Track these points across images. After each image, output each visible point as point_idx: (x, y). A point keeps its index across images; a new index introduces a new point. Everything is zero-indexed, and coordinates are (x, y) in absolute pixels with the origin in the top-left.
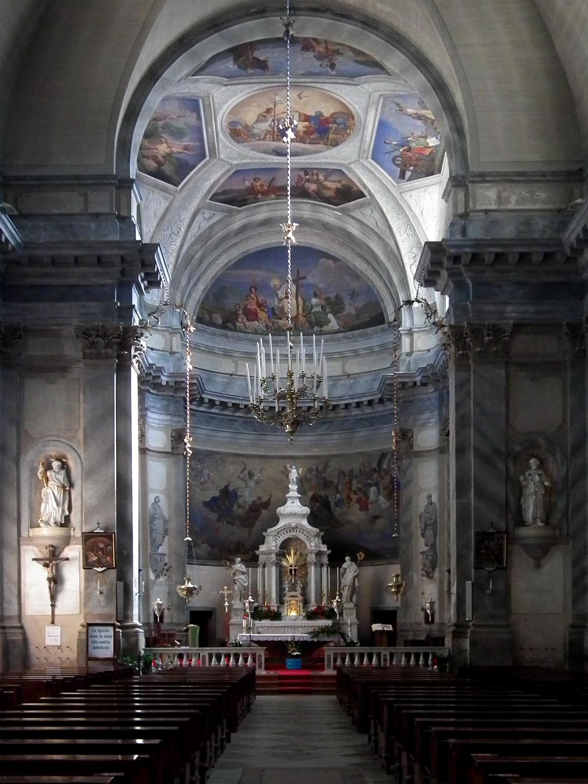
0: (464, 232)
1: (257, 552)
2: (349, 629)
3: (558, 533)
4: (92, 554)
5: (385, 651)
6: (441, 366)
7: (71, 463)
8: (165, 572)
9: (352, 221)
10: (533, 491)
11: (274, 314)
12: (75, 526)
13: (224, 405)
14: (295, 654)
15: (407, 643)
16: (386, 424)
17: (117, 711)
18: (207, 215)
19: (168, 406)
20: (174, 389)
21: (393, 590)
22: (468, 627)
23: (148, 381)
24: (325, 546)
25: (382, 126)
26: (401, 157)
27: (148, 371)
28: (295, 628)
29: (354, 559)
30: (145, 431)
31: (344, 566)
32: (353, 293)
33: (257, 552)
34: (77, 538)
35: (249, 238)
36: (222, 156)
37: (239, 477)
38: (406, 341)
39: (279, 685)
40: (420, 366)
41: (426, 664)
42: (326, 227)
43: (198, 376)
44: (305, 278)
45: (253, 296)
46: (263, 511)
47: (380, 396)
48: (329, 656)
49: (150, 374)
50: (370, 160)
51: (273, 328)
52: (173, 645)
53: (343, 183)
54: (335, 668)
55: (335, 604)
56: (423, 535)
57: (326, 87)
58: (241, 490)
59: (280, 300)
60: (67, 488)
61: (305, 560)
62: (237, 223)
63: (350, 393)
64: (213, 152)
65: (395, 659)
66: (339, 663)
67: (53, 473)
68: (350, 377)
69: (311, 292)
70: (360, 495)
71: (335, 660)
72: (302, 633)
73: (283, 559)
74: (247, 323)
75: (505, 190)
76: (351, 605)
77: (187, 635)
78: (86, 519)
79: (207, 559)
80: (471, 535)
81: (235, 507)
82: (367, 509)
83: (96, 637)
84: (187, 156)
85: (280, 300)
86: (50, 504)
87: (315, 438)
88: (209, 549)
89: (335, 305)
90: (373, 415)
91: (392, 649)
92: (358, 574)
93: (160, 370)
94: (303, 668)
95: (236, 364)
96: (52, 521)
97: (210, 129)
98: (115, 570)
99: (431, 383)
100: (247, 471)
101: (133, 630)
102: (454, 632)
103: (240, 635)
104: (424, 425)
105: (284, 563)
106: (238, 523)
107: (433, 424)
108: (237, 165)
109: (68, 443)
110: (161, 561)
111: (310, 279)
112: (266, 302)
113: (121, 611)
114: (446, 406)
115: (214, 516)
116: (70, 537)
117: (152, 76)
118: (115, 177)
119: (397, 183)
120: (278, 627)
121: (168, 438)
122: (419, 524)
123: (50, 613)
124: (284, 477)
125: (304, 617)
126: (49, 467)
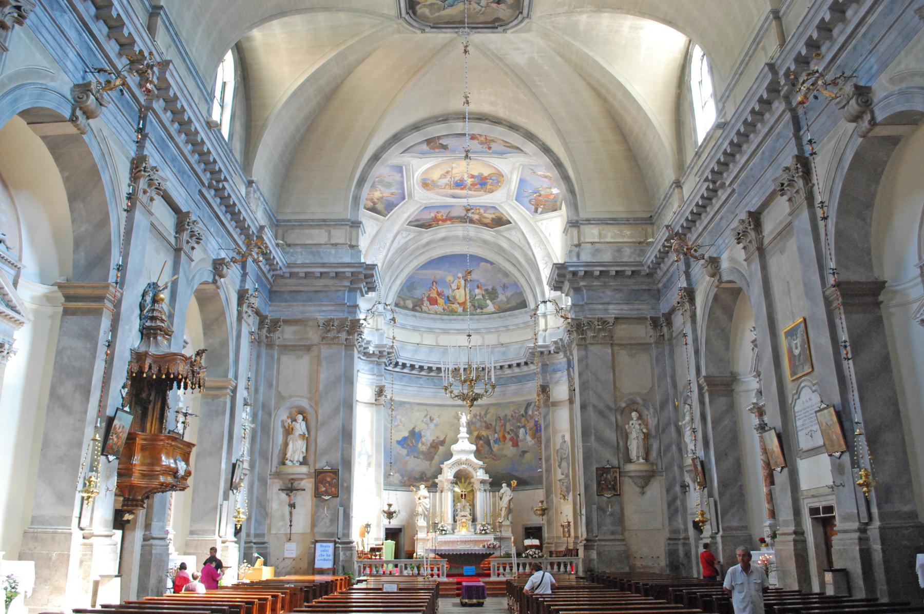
0: (578, 256)
1: (436, 480)
3: (655, 468)
9: (503, 239)
25: (522, 181)
29: (509, 485)
31: (502, 491)
36: (416, 198)
38: (542, 321)
42: (485, 242)
46: (440, 447)
47: (525, 360)
53: (497, 215)
57: (486, 159)
63: (504, 358)
64: (410, 196)
69: (475, 285)
70: (512, 435)
74: (431, 307)
75: (603, 230)
81: (420, 445)
84: (393, 199)
88: (401, 478)
89: (492, 294)
95: (422, 336)
100: (428, 417)
102: (585, 546)
104: (557, 382)
115: (404, 452)
117: (376, 158)
118: (349, 220)
124: (456, 421)
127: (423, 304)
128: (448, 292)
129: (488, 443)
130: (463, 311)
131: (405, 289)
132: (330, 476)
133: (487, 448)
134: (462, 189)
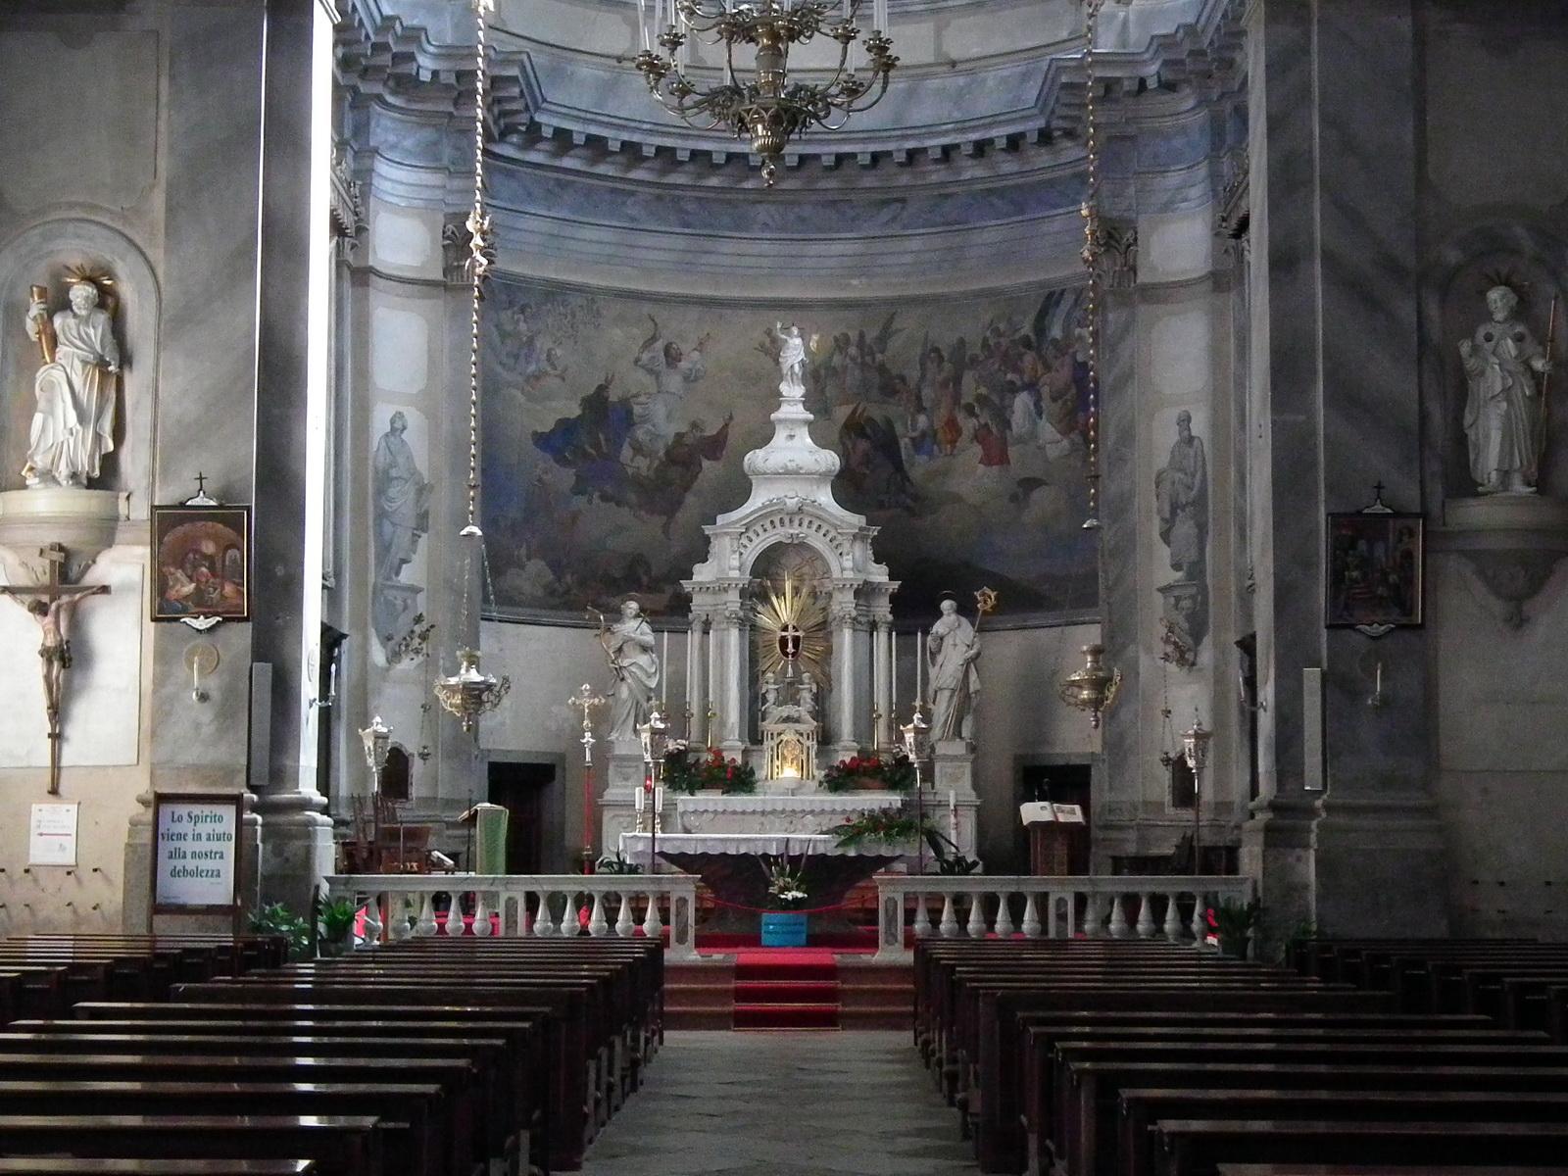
1: (687, 585)
2: (953, 820)
4: (179, 574)
5: (1062, 889)
6: (1218, 28)
7: (127, 291)
8: (417, 641)
10: (1498, 388)
12: (132, 485)
13: (596, 146)
14: (790, 896)
15: (1119, 865)
16: (1056, 206)
17: (236, 1087)
19: (435, 144)
20: (456, 93)
21: (1085, 694)
22: (1312, 813)
23: (380, 69)
24: (884, 568)
27: (380, 39)
28: (792, 816)
29: (966, 609)
30: (368, 216)
31: (939, 627)
33: (687, 585)
34: (136, 524)
37: (637, 361)
39: (742, 995)
40: (1156, 33)
41: (1186, 933)
43: (525, 57)
46: (706, 463)
47: (1041, 123)
48: (892, 901)
49: (385, 47)
52: (430, 865)
54: (910, 941)
55: (909, 737)
56: (1166, 536)
58: (642, 399)
60: (111, 368)
61: (824, 609)
63: (957, 115)
65: (1090, 915)
66: (920, 926)
67: (72, 321)
68: (959, 67)
70: (985, 417)
71: (910, 916)
72: (813, 833)
73: (760, 608)
76: (958, 748)
77: (470, 839)
78: (163, 466)
79: (542, 607)
80: (1318, 523)
81: (626, 452)
82: (1002, 459)
83: (182, 837)
86: (59, 412)
90: (1021, 181)
91: (1081, 883)
92: (978, 654)
93: (414, 35)
94: (814, 941)
96: (63, 471)
98: (249, 626)
99: (1188, 81)
100: (660, 345)
101: (298, 817)
102: (1269, 829)
103: (624, 839)
104: (1167, 207)
105: (765, 620)
106: (632, 497)
107: (1198, 202)
109: (120, 228)
110: (405, 608)
113: (262, 755)
114: (1231, 149)
115: (564, 478)
116: (116, 519)
120: (743, 813)
121: (433, 241)
122: (1155, 504)
123: (48, 762)
124: (769, 363)
125: (821, 783)
126: (59, 302)
132: (215, 537)
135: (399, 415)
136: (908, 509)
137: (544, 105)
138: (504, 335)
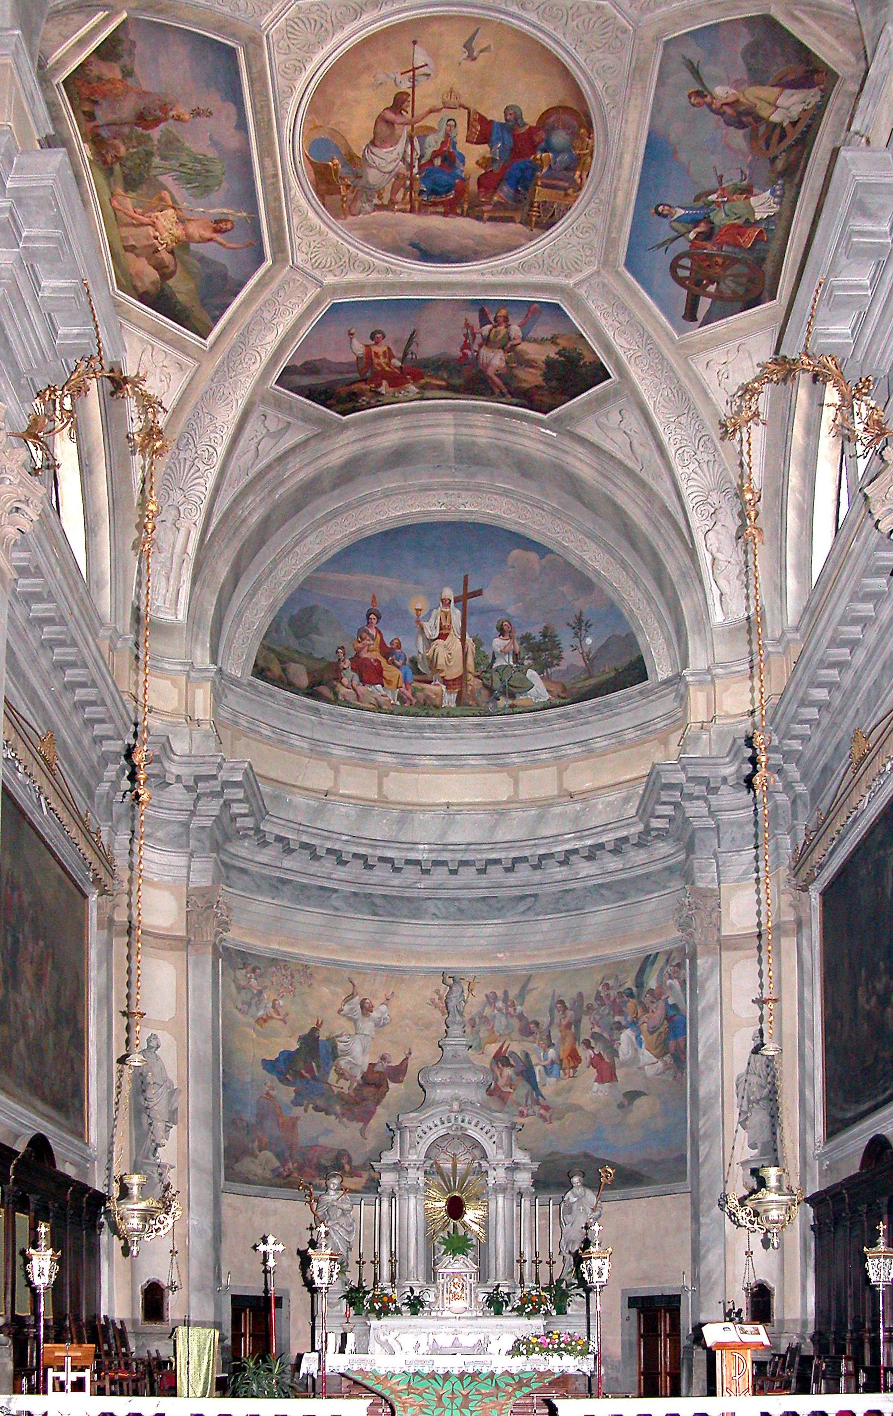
11: (417, 671)
16: (652, 892)
18: (273, 425)
26: (690, 257)
32: (579, 620)
35: (362, 502)
37: (340, 1011)
44: (479, 593)
45: (373, 632)
46: (391, 1085)
50: (622, 269)
51: (414, 701)
56: (743, 1123)
58: (344, 1038)
59: (430, 641)
62: (338, 454)
68: (576, 798)
69: (493, 626)
74: (361, 689)
81: (332, 1077)
82: (612, 1077)
85: (430, 641)
87: (501, 930)
88: (277, 1164)
95: (337, 771)
97: (268, 162)
100: (357, 1000)
106: (338, 1108)
108: (334, 290)
111: (489, 598)
112: (399, 646)
115: (285, 1093)
119: (680, 332)
127: (339, 679)
128: (413, 647)
129: (527, 1073)
130: (459, 701)
131: (285, 626)
133: (523, 1089)
134: (450, 210)
135: (155, 1036)
136: (541, 1116)
137: (267, 817)
138: (240, 988)
